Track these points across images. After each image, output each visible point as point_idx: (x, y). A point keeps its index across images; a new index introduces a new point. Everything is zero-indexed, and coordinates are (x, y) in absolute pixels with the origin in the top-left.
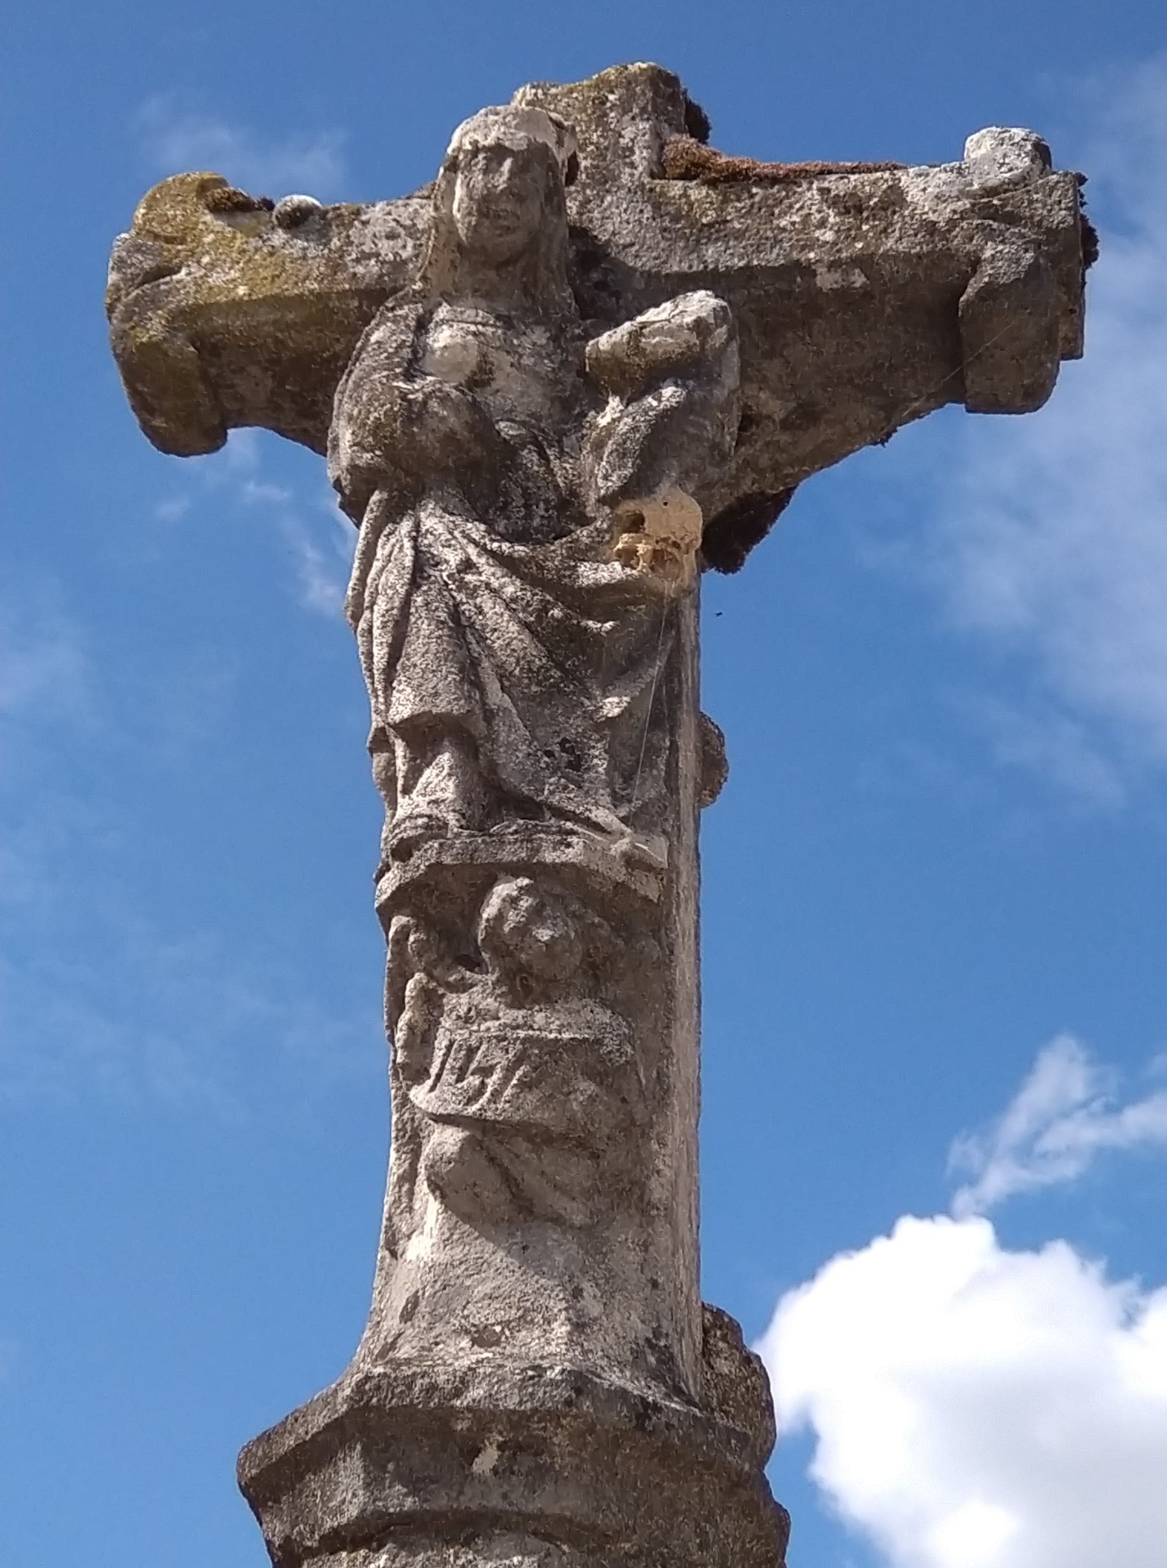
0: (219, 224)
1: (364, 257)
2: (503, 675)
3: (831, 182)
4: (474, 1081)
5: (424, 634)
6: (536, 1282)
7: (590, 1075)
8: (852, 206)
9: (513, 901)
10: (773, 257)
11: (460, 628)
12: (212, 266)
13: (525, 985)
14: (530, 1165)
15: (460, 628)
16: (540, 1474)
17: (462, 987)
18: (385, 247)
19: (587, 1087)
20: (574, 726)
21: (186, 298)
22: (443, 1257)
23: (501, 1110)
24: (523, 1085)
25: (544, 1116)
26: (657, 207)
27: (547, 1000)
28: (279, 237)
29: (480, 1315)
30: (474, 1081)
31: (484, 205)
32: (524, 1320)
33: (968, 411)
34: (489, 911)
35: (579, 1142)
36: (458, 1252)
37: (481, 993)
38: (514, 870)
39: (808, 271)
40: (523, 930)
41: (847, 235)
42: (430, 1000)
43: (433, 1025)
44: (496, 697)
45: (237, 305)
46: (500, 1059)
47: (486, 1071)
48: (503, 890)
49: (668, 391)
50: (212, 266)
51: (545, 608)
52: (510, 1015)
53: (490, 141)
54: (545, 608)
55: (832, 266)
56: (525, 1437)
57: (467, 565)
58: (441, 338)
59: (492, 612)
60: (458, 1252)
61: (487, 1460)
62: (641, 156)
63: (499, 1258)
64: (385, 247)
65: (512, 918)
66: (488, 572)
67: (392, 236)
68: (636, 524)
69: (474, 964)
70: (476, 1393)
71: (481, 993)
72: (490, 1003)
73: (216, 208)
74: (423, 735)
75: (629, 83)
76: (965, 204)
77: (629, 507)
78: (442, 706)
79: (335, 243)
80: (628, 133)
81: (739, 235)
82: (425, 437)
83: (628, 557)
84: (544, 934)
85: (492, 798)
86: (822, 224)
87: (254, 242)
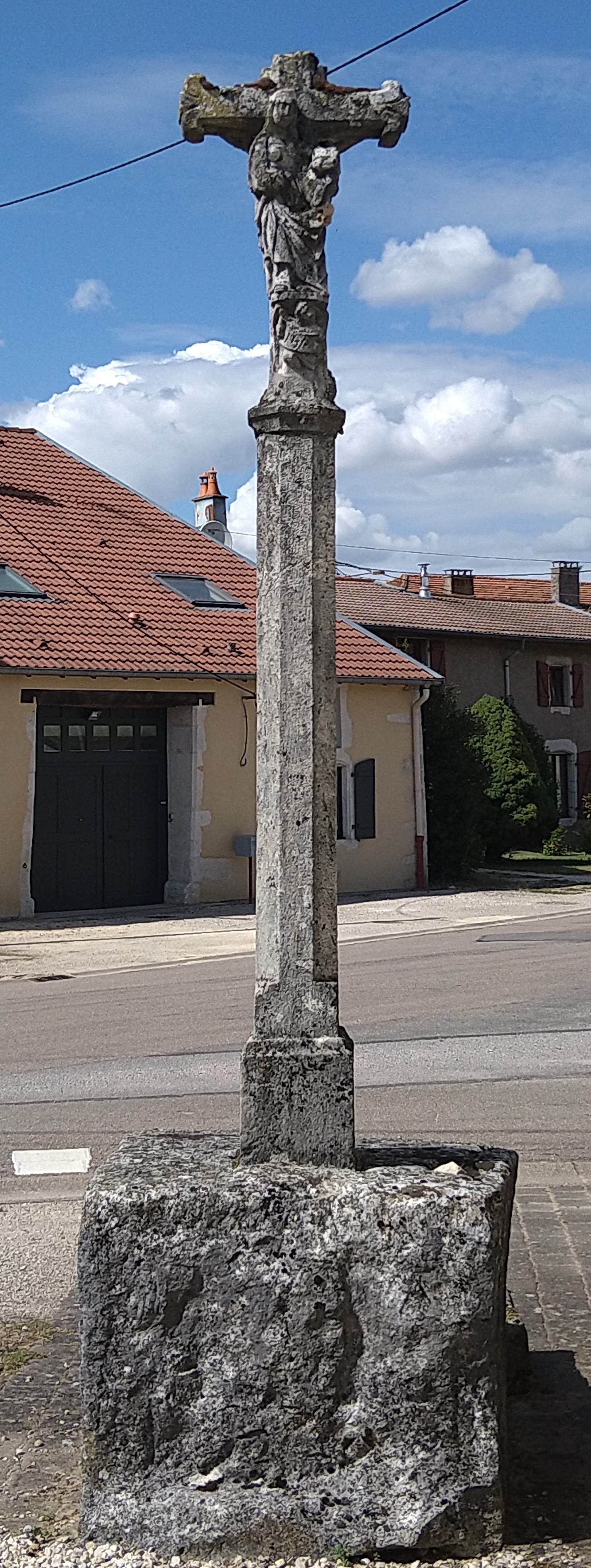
0: (206, 92)
1: (243, 107)
2: (295, 249)
3: (352, 95)
4: (294, 343)
5: (280, 241)
6: (307, 382)
7: (318, 342)
8: (357, 102)
9: (303, 307)
10: (340, 118)
11: (287, 238)
12: (206, 106)
13: (303, 323)
14: (305, 359)
15: (287, 238)
16: (312, 424)
17: (290, 320)
18: (248, 104)
19: (316, 344)
20: (310, 261)
21: (201, 115)
22: (287, 376)
23: (301, 350)
24: (305, 344)
25: (309, 351)
26: (313, 99)
27: (308, 325)
28: (222, 98)
29: (297, 389)
30: (294, 343)
31: (282, 117)
32: (305, 391)
33: (380, 145)
34: (298, 308)
35: (314, 354)
36: (290, 375)
37: (293, 322)
38: (303, 300)
39: (348, 121)
40: (305, 313)
41: (358, 112)
42: (284, 323)
43: (285, 328)
44: (295, 256)
45: (213, 118)
46: (301, 339)
47: (297, 341)
48: (301, 304)
49: (328, 178)
50: (206, 106)
51: (303, 232)
52: (301, 329)
53: (283, 101)
54: (303, 232)
55: (355, 121)
56: (309, 418)
57: (286, 221)
58: (272, 149)
59: (293, 234)
60: (290, 375)
61: (302, 421)
62: (308, 82)
63: (299, 376)
64: (248, 104)
65: (303, 311)
66: (290, 223)
67: (249, 101)
68: (321, 211)
69: (293, 316)
70: (301, 410)
71: (293, 322)
72: (297, 325)
73: (205, 88)
74: (281, 266)
75: (304, 57)
76: (384, 106)
77: (320, 208)
78: (286, 260)
79: (236, 102)
80: (304, 75)
81: (332, 110)
82: (275, 186)
83: (320, 219)
84: (309, 314)
85: (295, 280)
86: (351, 108)
87: (216, 100)
